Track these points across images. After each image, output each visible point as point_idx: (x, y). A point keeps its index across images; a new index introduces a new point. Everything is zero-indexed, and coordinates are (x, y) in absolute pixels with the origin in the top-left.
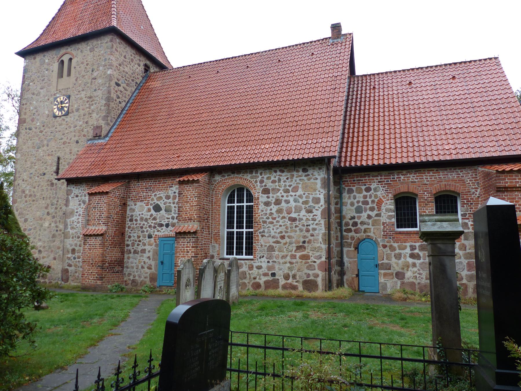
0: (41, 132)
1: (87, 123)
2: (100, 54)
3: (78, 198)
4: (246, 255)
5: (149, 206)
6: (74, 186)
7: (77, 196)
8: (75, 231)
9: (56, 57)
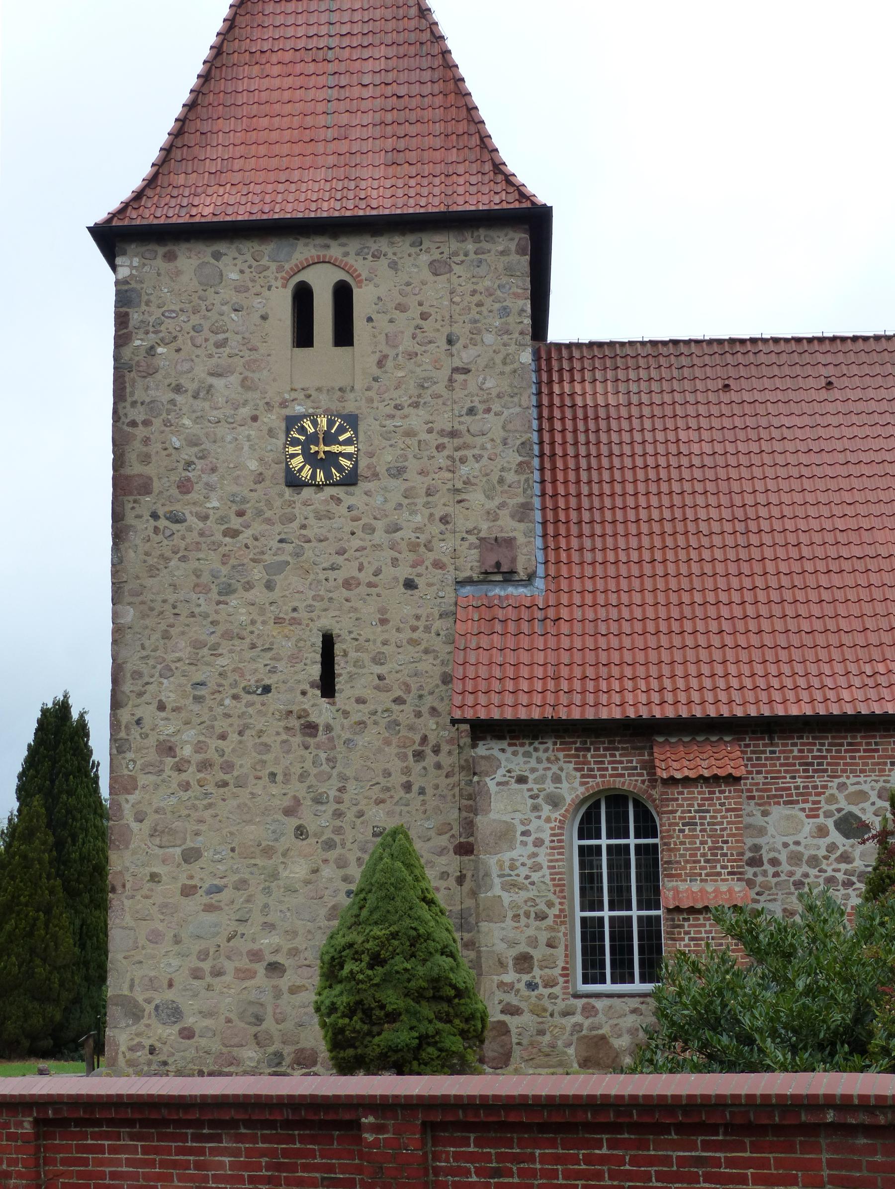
0: (233, 533)
1: (444, 520)
2: (479, 287)
3: (524, 787)
4: (614, 981)
5: (821, 820)
6: (504, 744)
7: (522, 780)
8: (524, 895)
9: (273, 266)
